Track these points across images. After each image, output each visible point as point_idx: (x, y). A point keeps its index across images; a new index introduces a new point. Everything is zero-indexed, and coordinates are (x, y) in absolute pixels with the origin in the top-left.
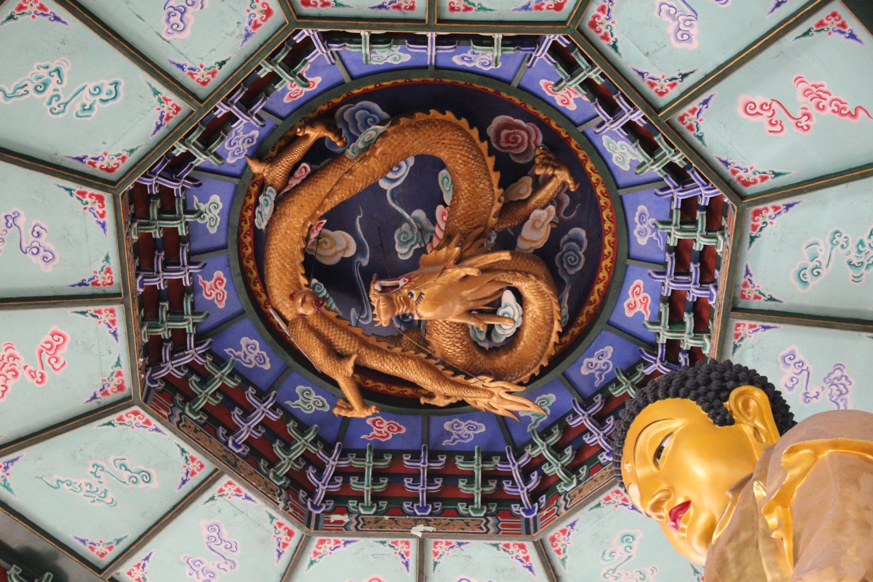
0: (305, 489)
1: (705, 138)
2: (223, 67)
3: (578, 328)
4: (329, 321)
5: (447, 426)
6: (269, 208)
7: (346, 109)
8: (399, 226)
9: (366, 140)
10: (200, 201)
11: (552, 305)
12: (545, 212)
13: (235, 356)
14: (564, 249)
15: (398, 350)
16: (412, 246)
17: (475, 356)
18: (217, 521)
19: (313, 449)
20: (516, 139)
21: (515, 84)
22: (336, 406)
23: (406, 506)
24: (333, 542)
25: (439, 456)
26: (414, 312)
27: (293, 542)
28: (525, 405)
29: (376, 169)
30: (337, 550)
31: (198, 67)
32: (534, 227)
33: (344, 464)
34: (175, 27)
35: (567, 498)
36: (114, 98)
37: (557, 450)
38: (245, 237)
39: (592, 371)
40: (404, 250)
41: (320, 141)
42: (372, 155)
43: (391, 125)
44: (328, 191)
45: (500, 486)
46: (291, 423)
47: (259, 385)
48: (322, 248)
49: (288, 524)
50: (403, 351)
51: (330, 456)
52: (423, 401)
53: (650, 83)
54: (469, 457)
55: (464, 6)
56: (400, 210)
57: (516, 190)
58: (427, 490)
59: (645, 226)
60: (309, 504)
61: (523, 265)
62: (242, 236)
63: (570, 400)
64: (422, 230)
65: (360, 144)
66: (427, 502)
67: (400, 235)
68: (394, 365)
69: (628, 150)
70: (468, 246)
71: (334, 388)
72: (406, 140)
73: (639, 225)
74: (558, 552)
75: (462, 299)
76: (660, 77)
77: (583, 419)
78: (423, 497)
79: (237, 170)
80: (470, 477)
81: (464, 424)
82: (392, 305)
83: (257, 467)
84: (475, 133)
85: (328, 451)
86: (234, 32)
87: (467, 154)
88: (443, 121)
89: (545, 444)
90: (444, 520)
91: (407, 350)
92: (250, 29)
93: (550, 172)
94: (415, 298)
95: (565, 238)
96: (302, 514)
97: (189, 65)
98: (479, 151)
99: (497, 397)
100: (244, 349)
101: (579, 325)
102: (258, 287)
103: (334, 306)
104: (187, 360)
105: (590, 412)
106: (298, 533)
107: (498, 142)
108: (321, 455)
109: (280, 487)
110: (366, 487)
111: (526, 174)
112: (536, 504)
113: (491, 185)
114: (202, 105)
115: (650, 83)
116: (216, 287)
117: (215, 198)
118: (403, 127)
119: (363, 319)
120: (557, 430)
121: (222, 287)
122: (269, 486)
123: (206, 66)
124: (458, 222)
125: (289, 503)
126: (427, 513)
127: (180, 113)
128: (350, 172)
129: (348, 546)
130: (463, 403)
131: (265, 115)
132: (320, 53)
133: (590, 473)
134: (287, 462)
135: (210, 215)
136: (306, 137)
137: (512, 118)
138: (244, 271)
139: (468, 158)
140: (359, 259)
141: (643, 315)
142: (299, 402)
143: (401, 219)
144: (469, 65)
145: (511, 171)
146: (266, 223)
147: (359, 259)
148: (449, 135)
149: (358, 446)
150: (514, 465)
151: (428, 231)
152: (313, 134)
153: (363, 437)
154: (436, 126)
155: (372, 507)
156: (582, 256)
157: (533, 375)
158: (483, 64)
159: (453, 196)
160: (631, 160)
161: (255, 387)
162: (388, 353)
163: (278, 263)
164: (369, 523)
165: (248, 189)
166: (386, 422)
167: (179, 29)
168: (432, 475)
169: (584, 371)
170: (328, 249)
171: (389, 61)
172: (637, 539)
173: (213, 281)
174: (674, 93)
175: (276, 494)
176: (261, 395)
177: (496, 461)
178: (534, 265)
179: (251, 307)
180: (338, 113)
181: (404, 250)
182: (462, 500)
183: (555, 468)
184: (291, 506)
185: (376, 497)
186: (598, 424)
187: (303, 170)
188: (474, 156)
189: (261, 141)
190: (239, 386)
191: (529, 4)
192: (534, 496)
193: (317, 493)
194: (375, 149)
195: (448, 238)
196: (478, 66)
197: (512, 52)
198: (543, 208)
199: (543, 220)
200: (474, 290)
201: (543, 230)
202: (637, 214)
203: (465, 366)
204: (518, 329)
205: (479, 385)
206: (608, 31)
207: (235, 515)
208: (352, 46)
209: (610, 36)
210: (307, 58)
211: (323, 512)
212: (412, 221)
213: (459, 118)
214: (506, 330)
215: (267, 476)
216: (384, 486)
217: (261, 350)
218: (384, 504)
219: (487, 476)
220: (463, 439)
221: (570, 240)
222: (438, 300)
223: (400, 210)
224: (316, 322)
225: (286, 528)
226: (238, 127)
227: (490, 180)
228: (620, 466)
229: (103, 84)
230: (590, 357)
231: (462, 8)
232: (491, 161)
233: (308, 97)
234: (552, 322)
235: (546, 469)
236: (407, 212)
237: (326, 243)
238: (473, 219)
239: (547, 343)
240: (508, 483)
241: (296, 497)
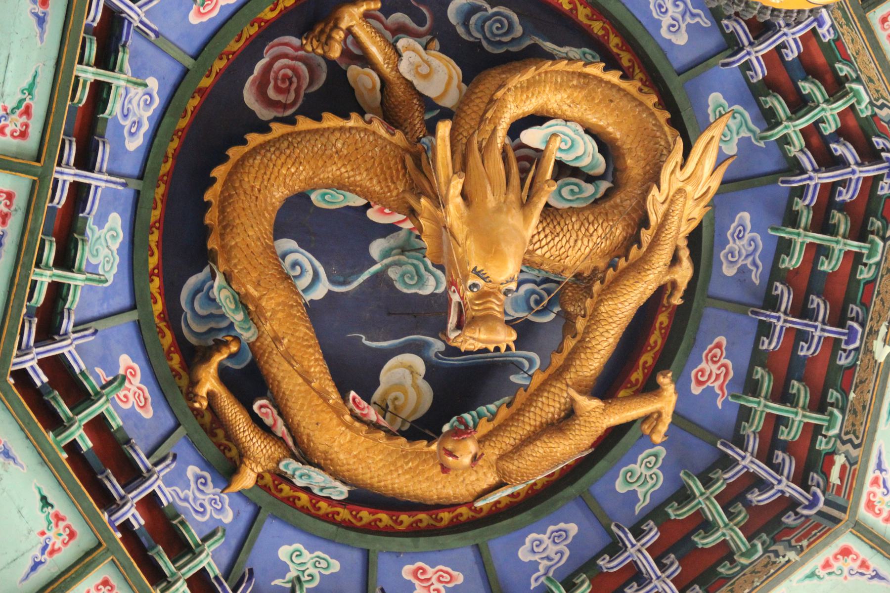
0: (783, 513)
2: (50, 500)
3: (612, 36)
4: (512, 419)
5: (729, 271)
6: (313, 475)
7: (188, 325)
8: (390, 283)
9: (233, 306)
10: (284, 578)
11: (557, 72)
12: (406, 55)
13: (545, 574)
14: (479, 36)
15: (580, 324)
16: (427, 269)
17: (616, 206)
19: (719, 487)
20: (285, 77)
21: (189, 62)
22: (649, 436)
23: (843, 362)
24: (875, 489)
25: (774, 293)
26: (504, 288)
27: (862, 550)
28: (708, 143)
29: (281, 300)
31: (42, 539)
32: (426, 77)
33: (753, 444)
35: (879, 103)
37: (800, 104)
38: (361, 519)
39: (683, 27)
40: (432, 282)
41: (224, 375)
42: (257, 302)
43: (216, 263)
44: (300, 380)
45: (844, 207)
46: (670, 511)
47: (598, 549)
48: (403, 406)
49: (829, 552)
50: (584, 316)
51: (735, 463)
52: (677, 301)
54: (785, 247)
55: (21, 115)
57: (365, 92)
58: (823, 323)
60: (806, 512)
61: (478, 103)
62: (359, 524)
63: (727, 71)
64: (403, 249)
65: (238, 317)
66: (843, 326)
67: (405, 284)
68: (601, 335)
70: (427, 185)
71: (630, 433)
72: (244, 247)
75: (498, 210)
77: (756, 54)
78: (832, 332)
79: (247, 511)
80: (817, 252)
81: (731, 244)
82: (486, 319)
83: (728, 578)
84: (254, 139)
85: (726, 463)
87: (283, 157)
88: (225, 184)
89: (785, 123)
90: (875, 306)
91: (585, 309)
93: (339, 35)
94: (481, 282)
95: (460, 30)
96: (817, 526)
97: (37, 552)
98: (284, 137)
99: (686, 187)
100: (536, 558)
101: (607, 34)
102: (446, 516)
103: (492, 407)
105: (746, 43)
106: (847, 539)
107: (285, 107)
108: (731, 476)
109: (766, 551)
110: (799, 417)
111: (345, 72)
112: (883, 154)
113: (341, 129)
114: (104, 544)
116: (429, 580)
117: (284, 553)
118: (223, 247)
119: (530, 368)
120: (768, 99)
121: (430, 571)
122: (758, 568)
123: (43, 526)
124: (390, 191)
125: (793, 543)
126: (860, 330)
127: (113, 581)
128: (276, 339)
129: (886, 465)
130: (694, 239)
131: (159, 453)
132: (72, 348)
133: (847, 60)
134: (728, 531)
135: (309, 565)
136: (211, 395)
137: (251, 78)
138: (415, 532)
139: (289, 156)
140: (432, 353)
142: (641, 492)
143: (380, 278)
144: (146, 127)
145: (334, 95)
146: (338, 484)
147: (432, 353)
148: (249, 179)
149: (732, 415)
150: (810, 178)
151: (408, 241)
152: (209, 381)
153: (719, 405)
154: (230, 196)
155: (831, 414)
156: (495, 9)
157: (670, 122)
158: (148, 105)
159: (350, 191)
161: (599, 555)
162: (582, 340)
163: (403, 479)
164: (853, 425)
165: (277, 499)
166: (703, 365)
168: (802, 310)
169: (681, 39)
170: (406, 399)
171: (115, 246)
173: (416, 582)
175: (773, 559)
176: (614, 548)
177: (800, 205)
178: (481, 87)
179: (471, 533)
180: (193, 340)
181: (432, 282)
182: (854, 270)
183: (828, 114)
184: (799, 540)
185: (819, 405)
186: (770, 33)
187: (264, 410)
188: (288, 148)
189: (207, 465)
190: (592, 582)
191: (36, 15)
192: (870, 155)
193: (791, 497)
194: (247, 294)
195: (412, 213)
196: (150, 113)
197: (127, 57)
198: (400, 56)
199: (417, 59)
200: (489, 188)
201: (435, 62)
203: (628, 225)
204: (587, 131)
205: (662, 209)
208: (70, 298)
210: (77, 371)
211: (824, 493)
212: (386, 261)
213: (226, 158)
214: (585, 153)
215: (744, 567)
216: (802, 388)
217: (545, 533)
218: (833, 395)
219: (822, 225)
220: (755, 250)
221: (466, 24)
222: (492, 247)
224: (508, 440)
225: (835, 558)
226: (167, 496)
227: (333, 130)
228: (779, 11)
230: (661, 27)
231: (24, 119)
232: (305, 124)
233: (151, 380)
234: (586, 76)
235: (829, 129)
236: (371, 266)
237: (396, 399)
238: (389, 168)
239: (620, 89)
240: (840, 193)
241: (790, 529)
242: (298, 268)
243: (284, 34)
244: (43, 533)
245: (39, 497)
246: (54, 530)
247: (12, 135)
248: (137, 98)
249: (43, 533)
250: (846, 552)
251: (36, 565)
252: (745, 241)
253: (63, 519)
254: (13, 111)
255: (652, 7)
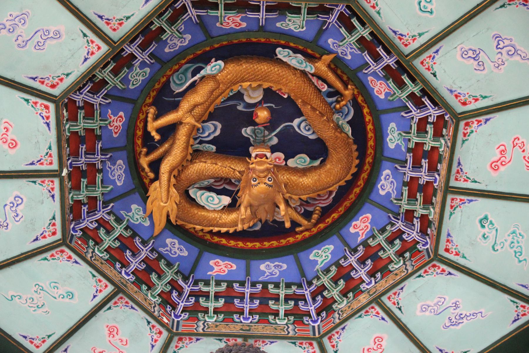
1: (360, 319)
2: (432, 75)
9: (344, 125)
16: (252, 136)
18: (64, 37)
30: (41, 118)
31: (435, 61)
34: (466, 53)
36: (421, 9)
53: (396, 293)
55: (454, 206)
56: (278, 130)
59: (273, 268)
69: (325, 260)
73: (273, 265)
74: (52, 255)
76: (400, 297)
81: (122, 172)
86: (455, 84)
92: (456, 93)
97: (437, 57)
104: (98, 216)
115: (396, 293)
123: (434, 66)
141: (212, 271)
142: (138, 70)
160: (317, 261)
166: (121, 124)
167: (463, 55)
169: (168, 241)
172: (71, 301)
174: (389, 304)
187: (323, 87)
191: (451, 237)
202: (281, 264)
206: (430, 273)
207: (70, 50)
209: (426, 274)
212: (270, 136)
223: (278, 130)
229: (432, 4)
242: (307, 129)
243: (325, 207)
244: (435, 63)
245: (437, 76)
246: (430, 65)
247: (457, 199)
248: (388, 188)
249: (435, 63)
250: (53, 86)
251: (437, 52)
252: (116, 175)
253: (426, 69)
254: (457, 206)
255: (184, 249)
